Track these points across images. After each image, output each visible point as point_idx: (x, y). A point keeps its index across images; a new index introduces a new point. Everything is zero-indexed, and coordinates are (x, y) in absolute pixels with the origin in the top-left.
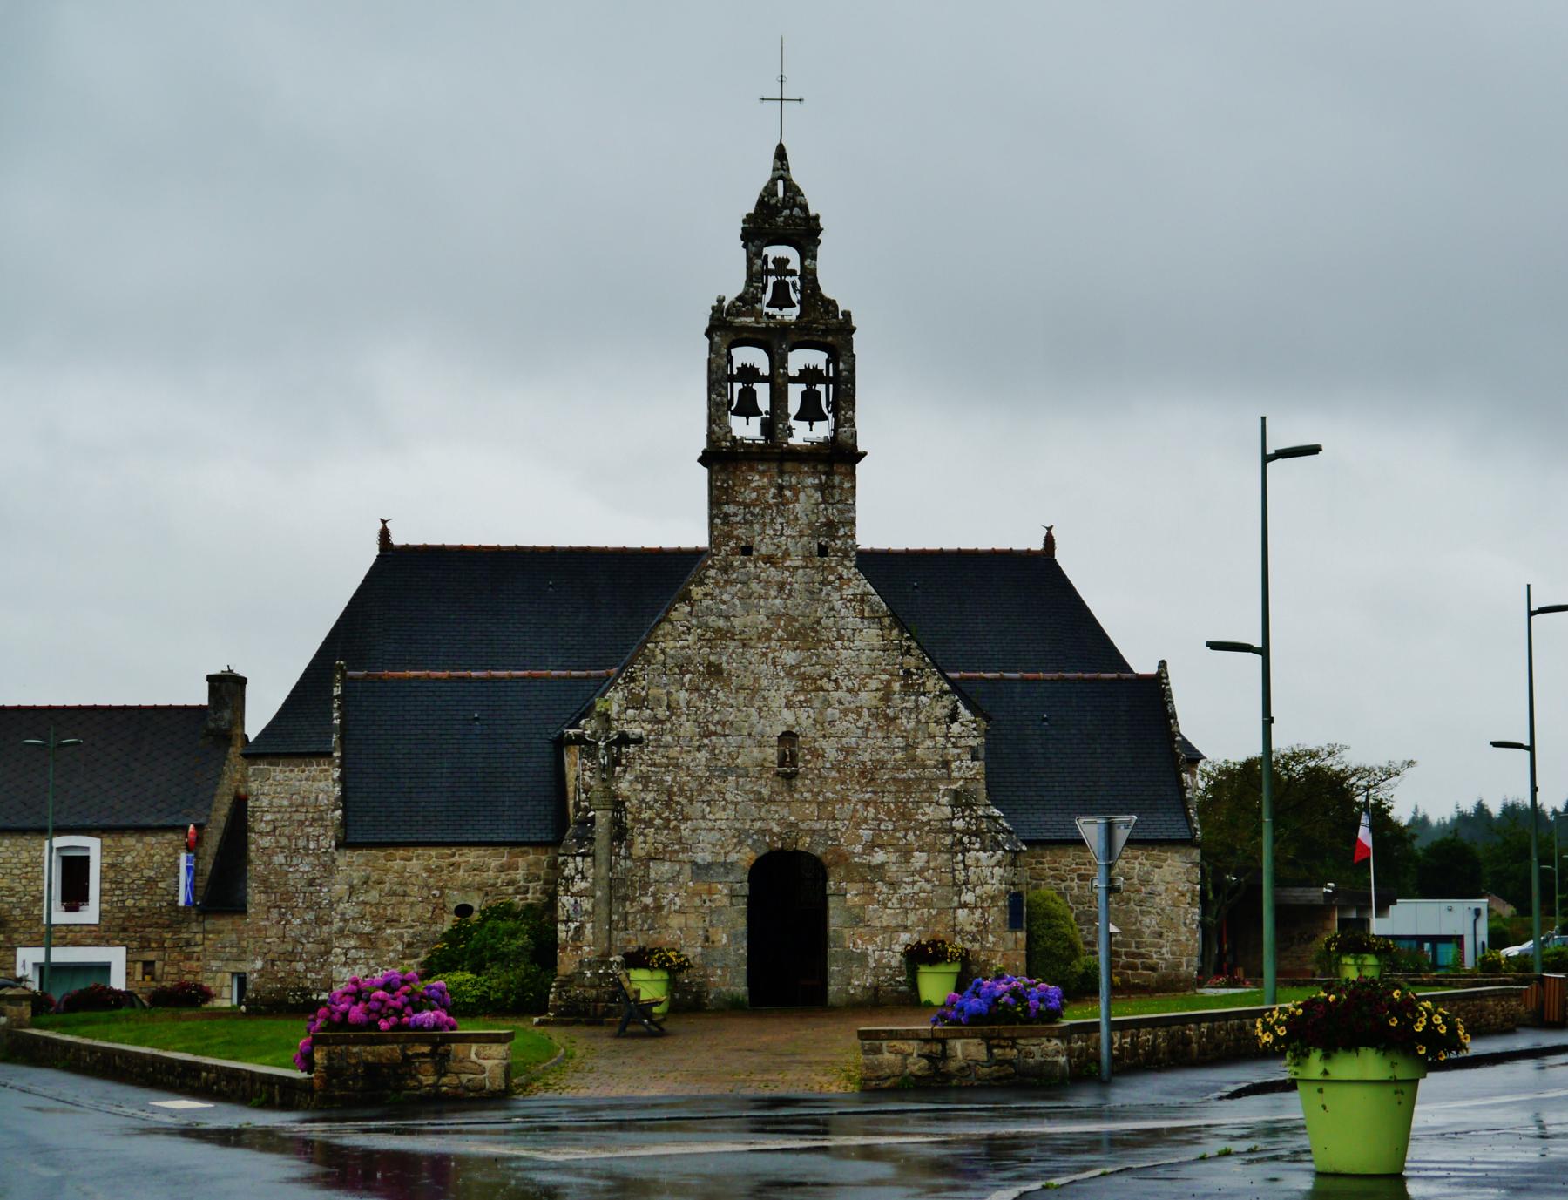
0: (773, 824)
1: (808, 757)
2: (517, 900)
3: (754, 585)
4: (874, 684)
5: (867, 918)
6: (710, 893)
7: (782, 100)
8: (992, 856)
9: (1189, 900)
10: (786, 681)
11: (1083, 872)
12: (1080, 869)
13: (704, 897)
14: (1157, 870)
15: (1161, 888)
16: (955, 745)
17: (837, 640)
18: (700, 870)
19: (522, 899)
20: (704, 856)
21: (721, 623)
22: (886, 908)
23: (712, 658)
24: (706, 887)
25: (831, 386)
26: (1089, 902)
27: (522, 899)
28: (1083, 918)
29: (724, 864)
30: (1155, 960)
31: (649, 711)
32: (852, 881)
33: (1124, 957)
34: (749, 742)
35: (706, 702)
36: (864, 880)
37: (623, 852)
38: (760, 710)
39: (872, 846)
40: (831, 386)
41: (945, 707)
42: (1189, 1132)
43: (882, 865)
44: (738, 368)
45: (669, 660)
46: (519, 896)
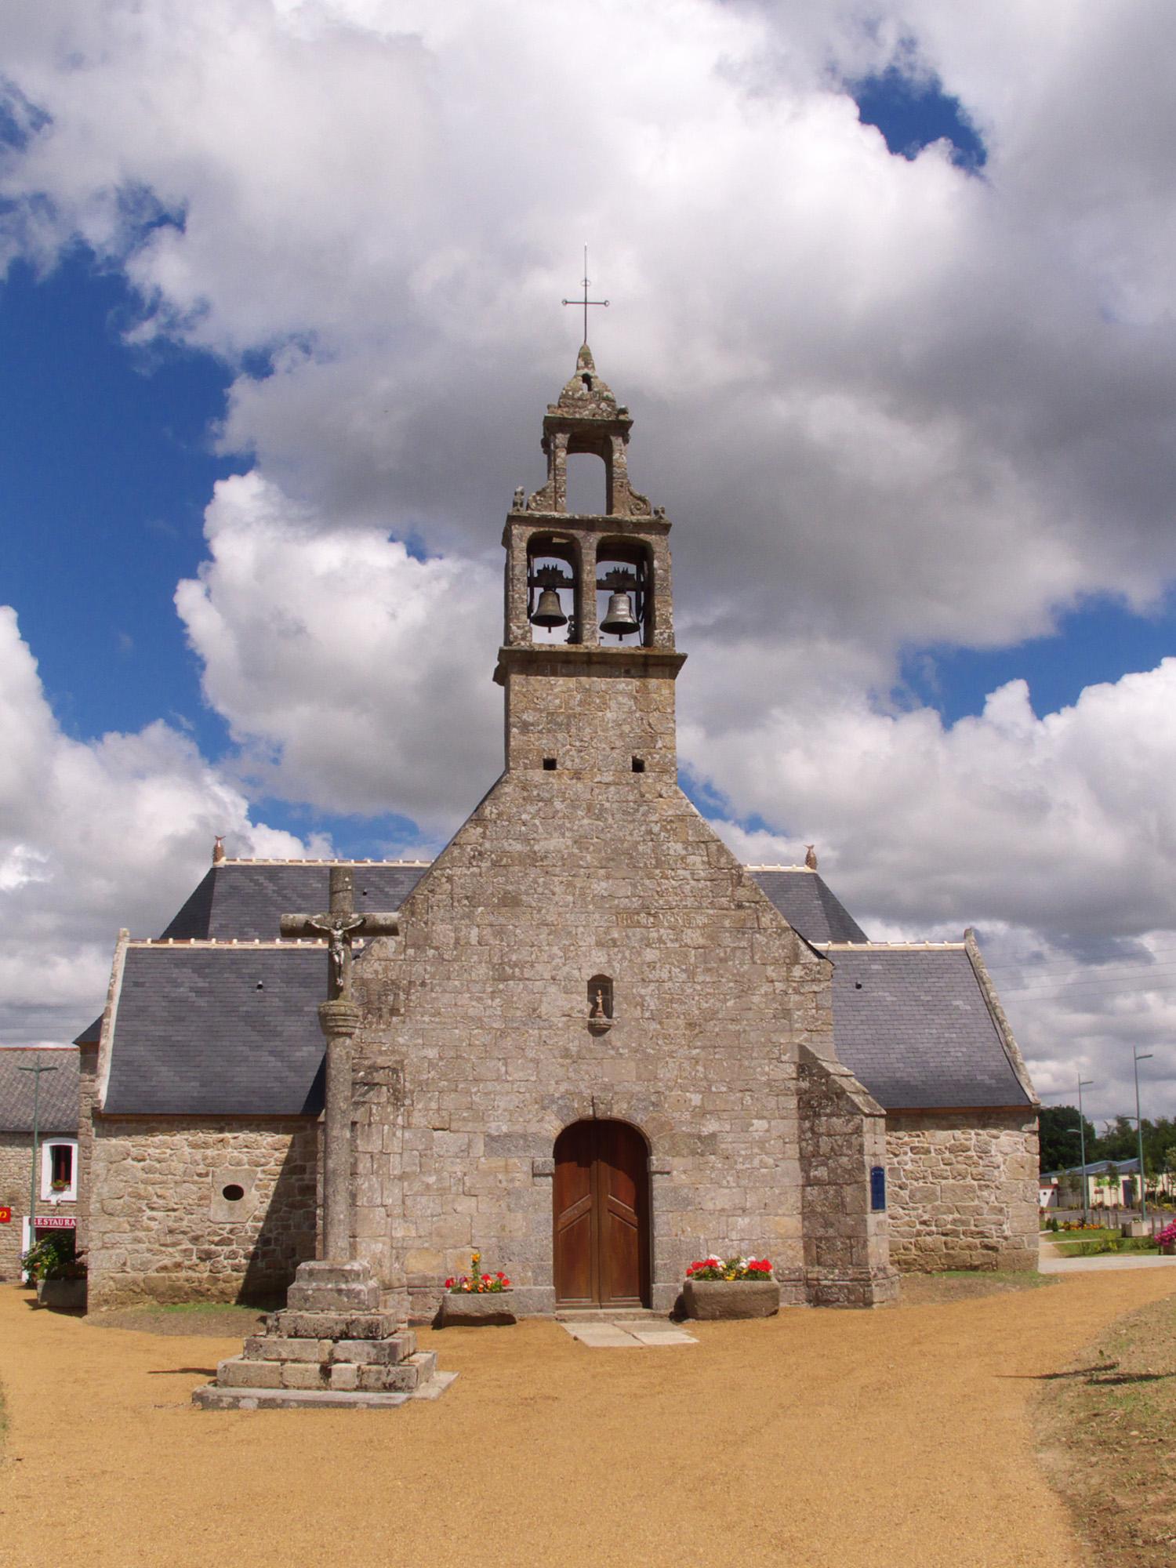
0: (582, 1086)
1: (625, 1006)
2: (292, 1181)
3: (558, 805)
4: (701, 920)
5: (698, 1200)
6: (506, 1169)
7: (586, 303)
8: (849, 1121)
9: (1028, 1172)
10: (597, 916)
11: (917, 1145)
12: (913, 1142)
13: (500, 1177)
14: (994, 1140)
15: (1000, 1159)
16: (797, 991)
17: (656, 867)
18: (494, 1142)
19: (298, 1180)
20: (499, 1126)
21: (518, 847)
22: (721, 1187)
23: (510, 888)
24: (502, 1163)
25: (642, 593)
26: (924, 1178)
27: (298, 1180)
28: (918, 1195)
29: (524, 1136)
30: (995, 1239)
31: (432, 951)
32: (678, 1154)
33: (962, 1237)
34: (553, 989)
35: (502, 940)
36: (694, 1153)
37: (400, 1120)
38: (565, 949)
39: (702, 1113)
40: (642, 593)
41: (784, 947)
42: (316, 954)
43: (713, 1136)
44: (539, 571)
45: (457, 890)
46: (295, 1177)
